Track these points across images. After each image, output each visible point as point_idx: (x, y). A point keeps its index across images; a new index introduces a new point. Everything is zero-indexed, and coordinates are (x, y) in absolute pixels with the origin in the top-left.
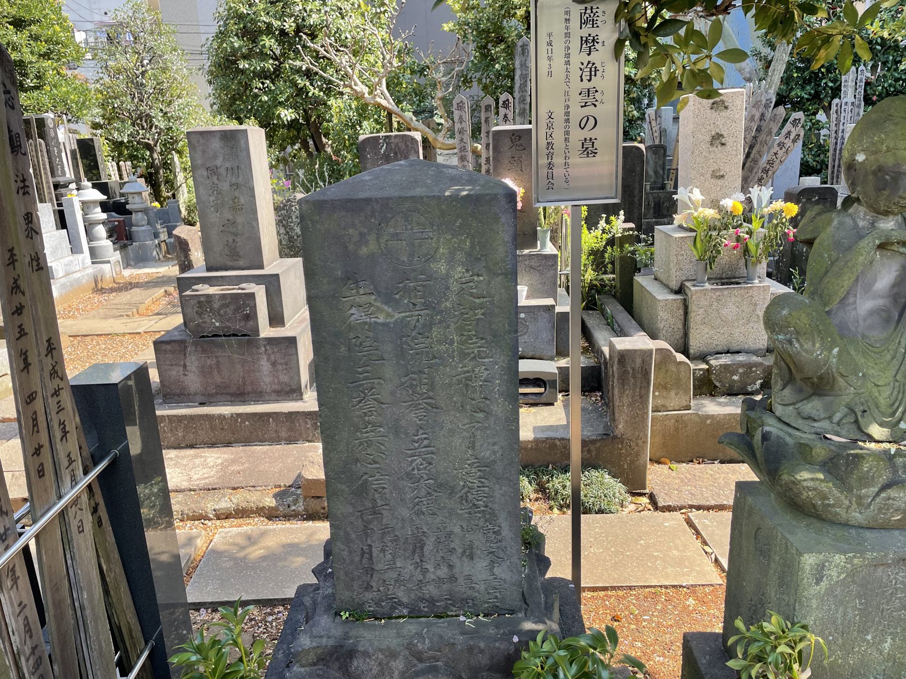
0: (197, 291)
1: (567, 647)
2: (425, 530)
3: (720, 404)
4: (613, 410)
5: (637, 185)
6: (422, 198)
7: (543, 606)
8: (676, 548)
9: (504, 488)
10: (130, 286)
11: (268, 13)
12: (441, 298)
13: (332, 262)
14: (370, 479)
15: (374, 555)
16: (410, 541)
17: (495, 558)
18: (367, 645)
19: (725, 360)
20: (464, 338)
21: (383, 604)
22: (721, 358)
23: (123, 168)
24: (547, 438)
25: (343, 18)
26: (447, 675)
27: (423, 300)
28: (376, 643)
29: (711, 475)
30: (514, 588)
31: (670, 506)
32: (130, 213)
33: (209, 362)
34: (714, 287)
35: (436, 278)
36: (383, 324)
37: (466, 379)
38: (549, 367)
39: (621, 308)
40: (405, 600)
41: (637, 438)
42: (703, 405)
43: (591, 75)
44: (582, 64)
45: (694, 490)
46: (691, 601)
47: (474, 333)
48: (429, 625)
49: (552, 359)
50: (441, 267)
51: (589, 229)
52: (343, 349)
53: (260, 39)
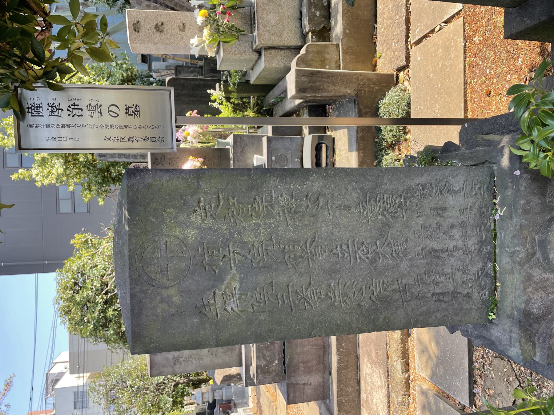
0: (254, 375)
1: (530, 128)
2: (420, 248)
3: (336, 24)
4: (337, 96)
5: (193, 82)
6: (130, 250)
7: (486, 148)
8: (436, 51)
9: (385, 181)
10: (258, 404)
11: (93, 312)
12: (218, 234)
13: (186, 327)
14: (375, 294)
15: (441, 291)
16: (429, 261)
17: (446, 189)
18: (519, 300)
19: (306, 21)
20: (254, 214)
21: (483, 283)
22: (305, 24)
23: (188, 402)
24: (357, 142)
25: (97, 266)
26: (548, 232)
27: (221, 249)
28: (518, 292)
29: (385, 29)
30: (472, 173)
31: (406, 57)
32: (215, 400)
33: (302, 368)
34: (256, 29)
35: (201, 238)
36: (241, 283)
37: (289, 212)
38: (308, 140)
39: (271, 93)
40: (480, 265)
41: (357, 80)
42: (337, 35)
43: (78, 109)
44: (69, 115)
45: (395, 41)
46: (476, 39)
47: (250, 206)
48: (503, 246)
49: (303, 139)
50: (191, 234)
51: (221, 112)
52: (262, 317)
53: (108, 317)
